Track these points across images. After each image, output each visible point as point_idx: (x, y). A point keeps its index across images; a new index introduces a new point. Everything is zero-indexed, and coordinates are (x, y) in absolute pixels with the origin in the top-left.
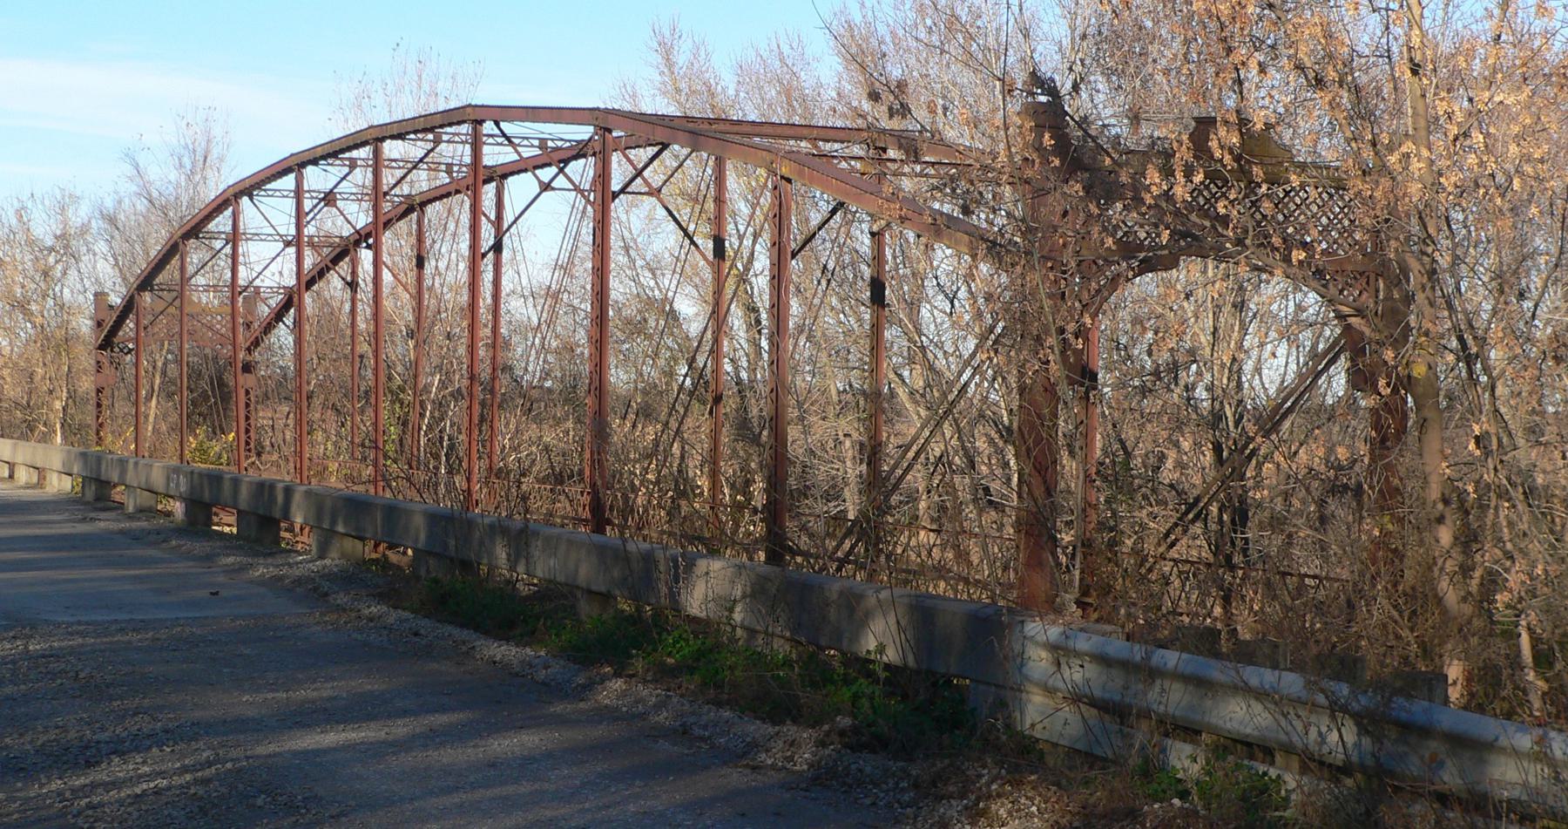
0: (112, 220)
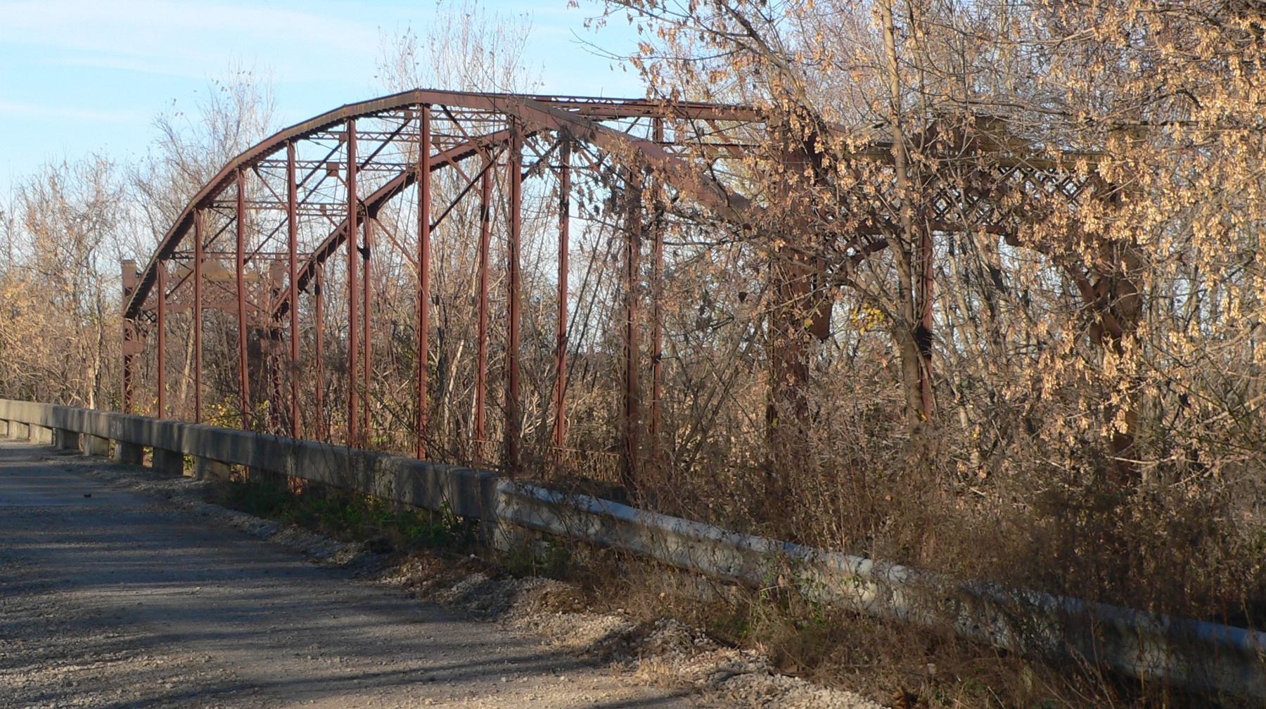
0: (145, 188)
